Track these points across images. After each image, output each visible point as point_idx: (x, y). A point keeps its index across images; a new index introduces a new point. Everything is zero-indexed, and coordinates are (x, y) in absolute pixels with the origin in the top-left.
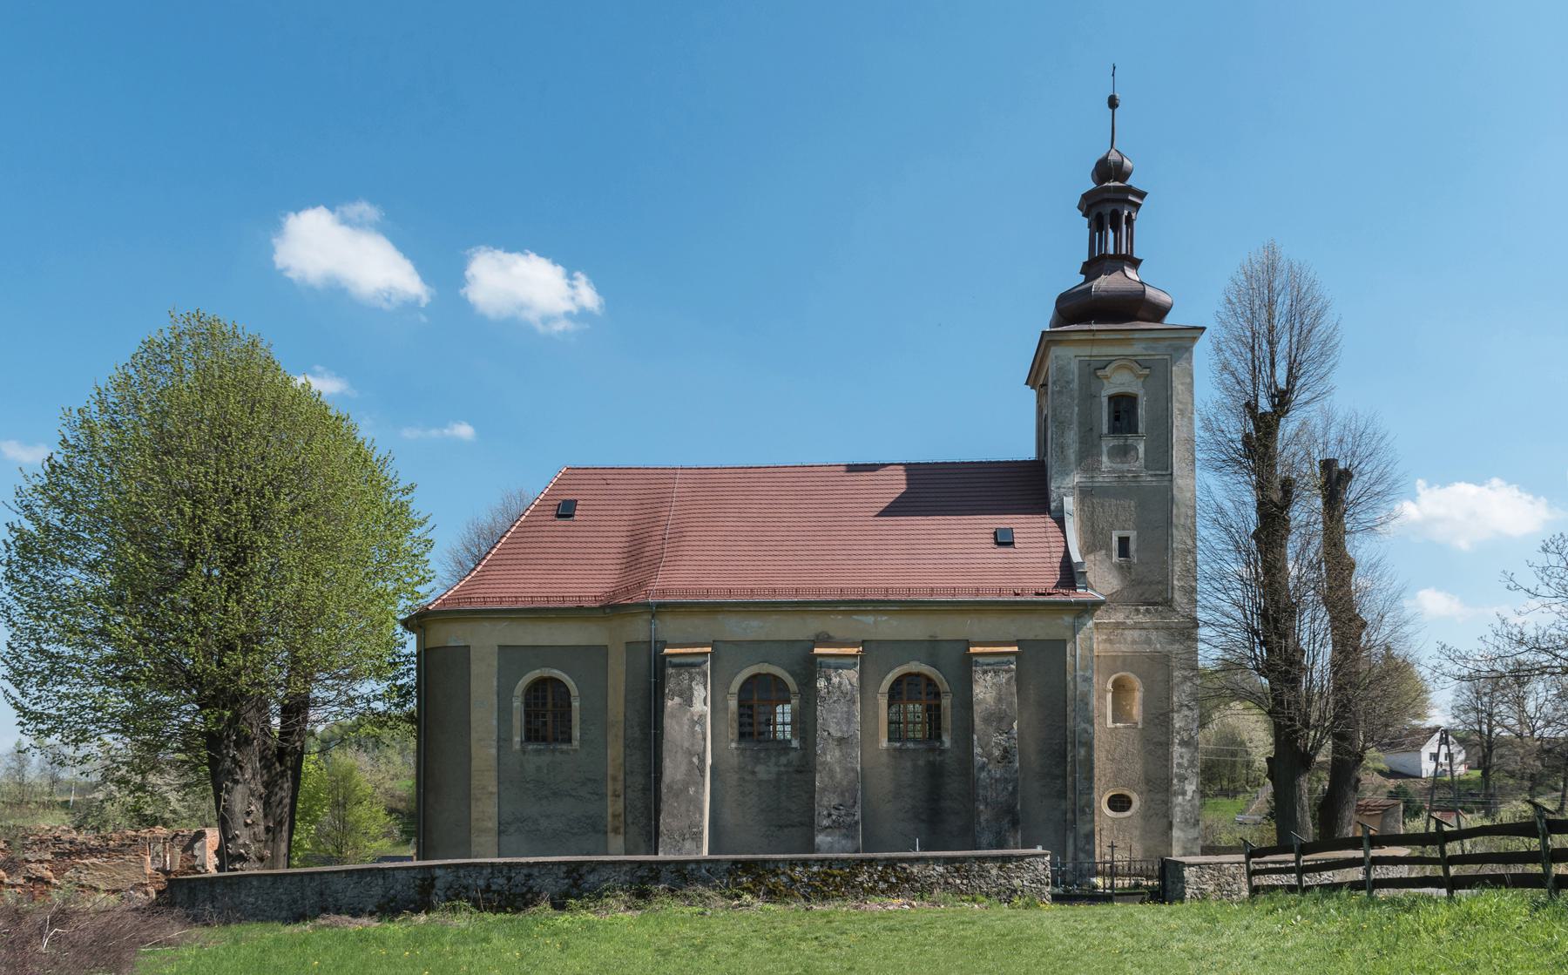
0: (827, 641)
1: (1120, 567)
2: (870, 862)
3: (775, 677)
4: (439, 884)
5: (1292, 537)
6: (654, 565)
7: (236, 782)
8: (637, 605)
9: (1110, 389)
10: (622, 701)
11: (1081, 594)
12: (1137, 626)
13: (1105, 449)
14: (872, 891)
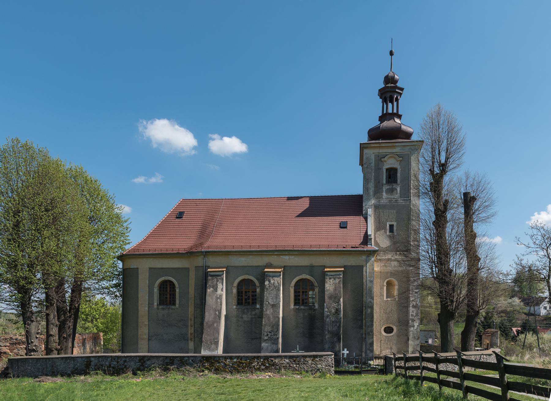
0: (270, 266)
1: (390, 237)
2: (258, 357)
3: (251, 280)
4: (92, 364)
5: (448, 224)
6: (208, 237)
7: (32, 321)
8: (198, 252)
9: (386, 166)
10: (193, 289)
11: (369, 247)
12: (396, 260)
13: (384, 190)
14: (259, 369)
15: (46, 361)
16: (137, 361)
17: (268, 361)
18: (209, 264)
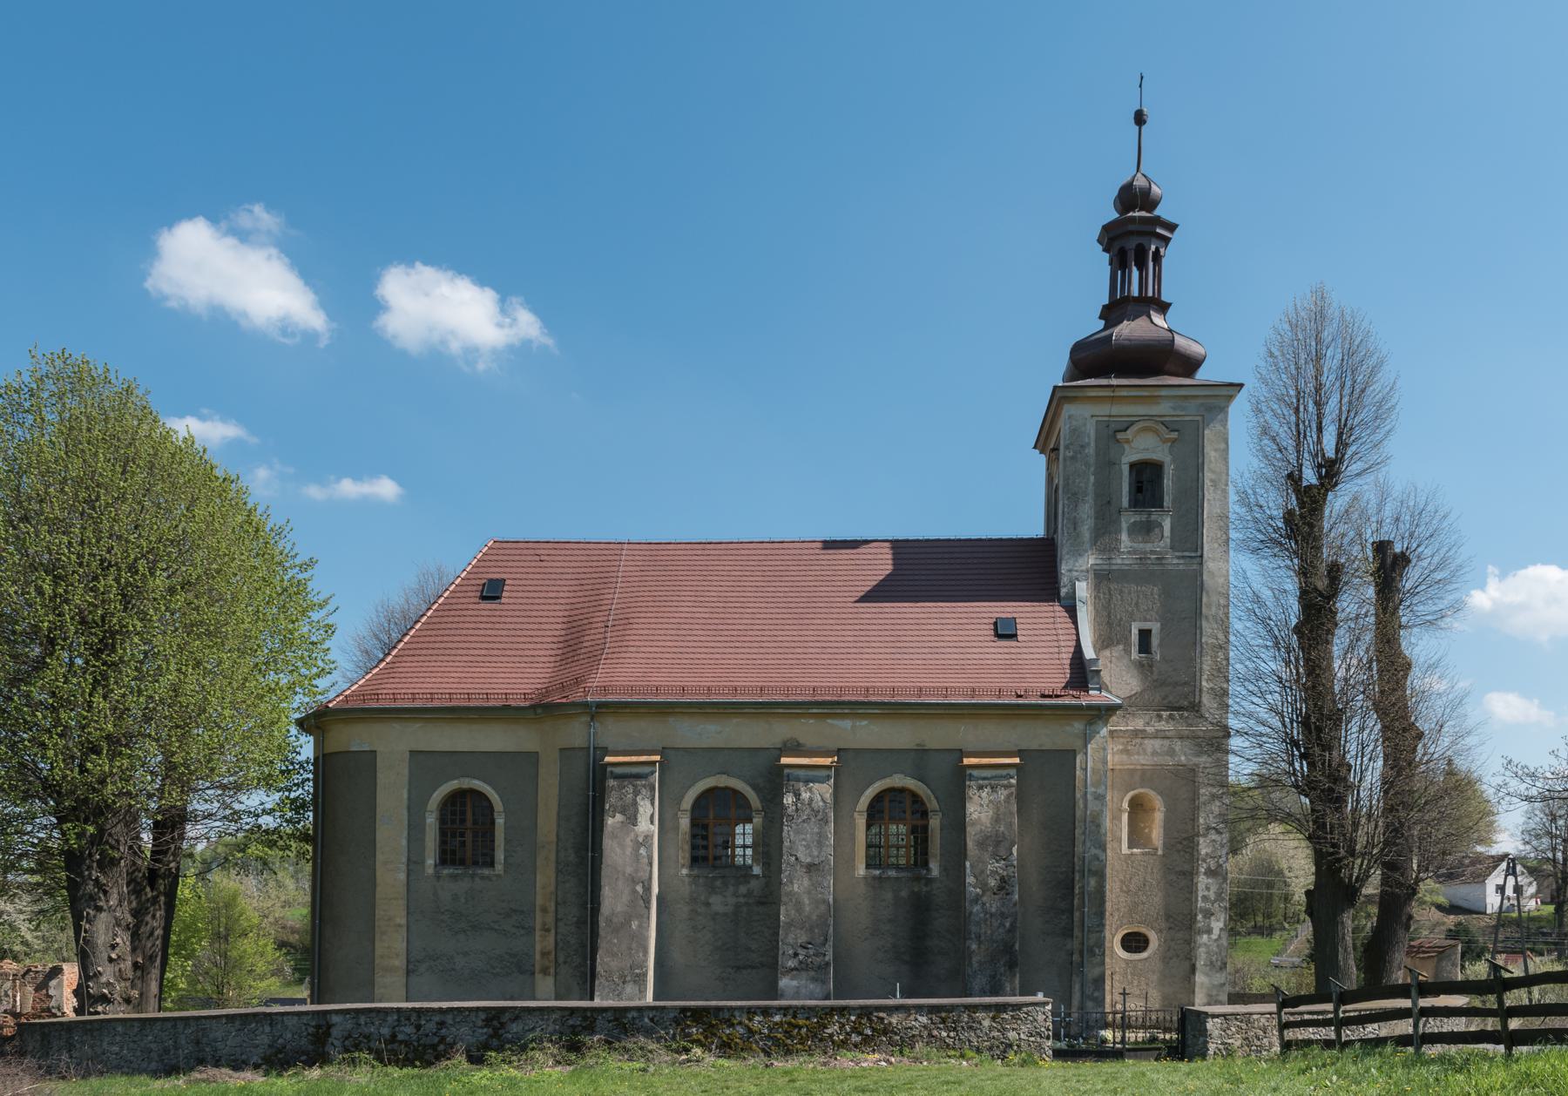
0: (796, 749)
1: (1140, 666)
2: (842, 1011)
3: (735, 792)
4: (335, 1032)
5: (1340, 632)
6: (594, 658)
7: (99, 909)
8: (574, 704)
9: (1131, 455)
11: (1094, 697)
13: (1124, 525)
14: (843, 1044)
15: (174, 1026)
16: (480, 1023)
17: (870, 1020)
18: (605, 740)
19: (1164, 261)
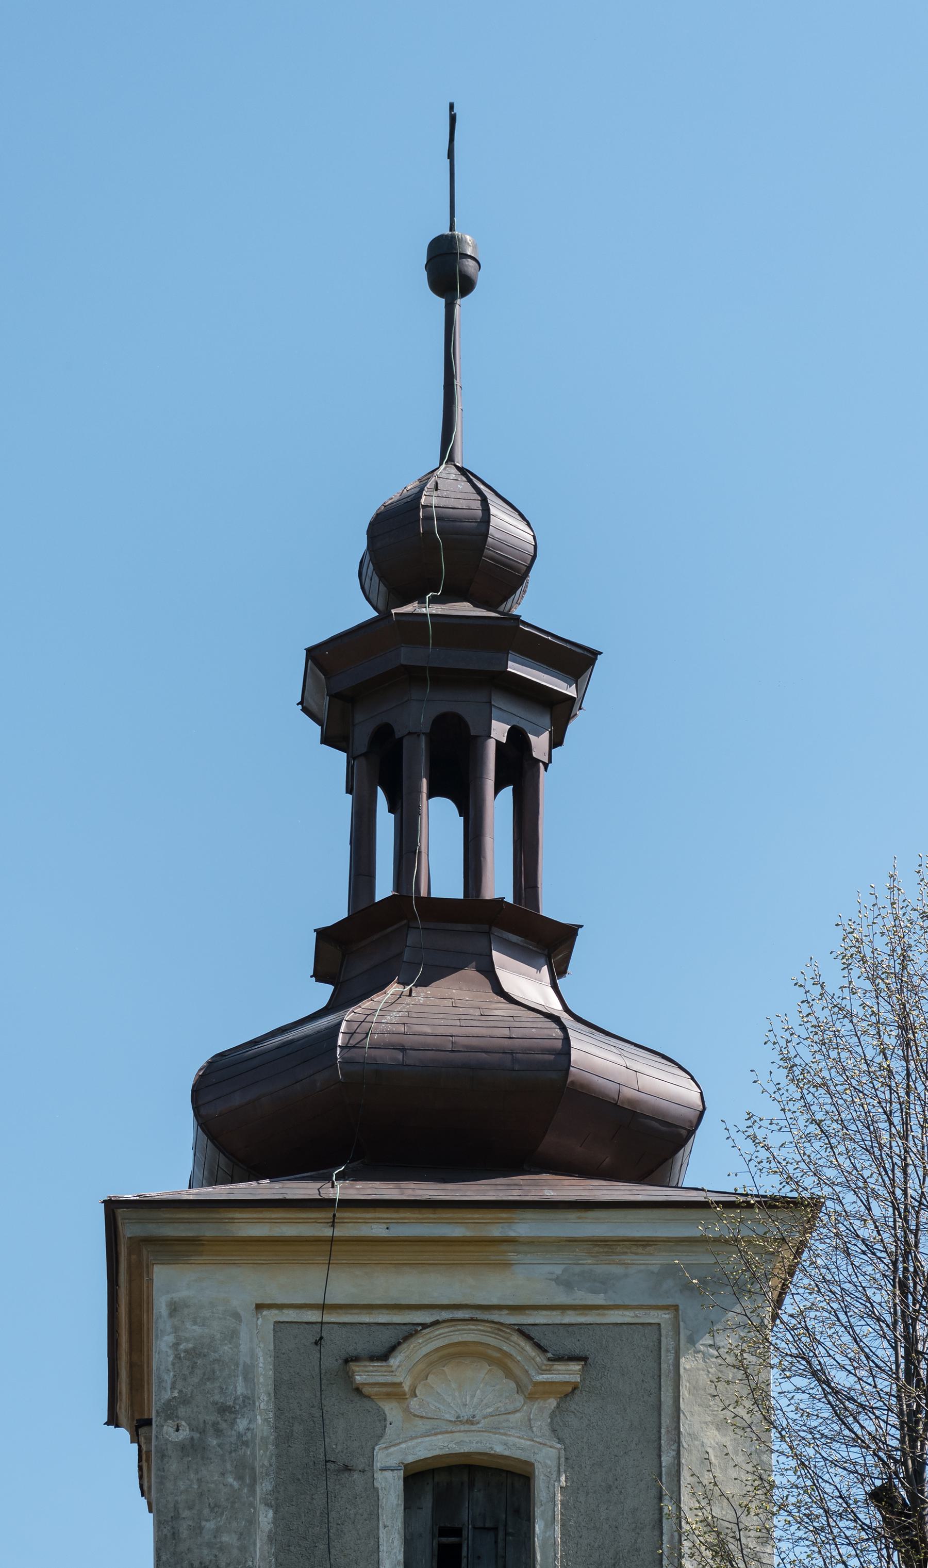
9: (410, 1441)
19: (549, 784)
